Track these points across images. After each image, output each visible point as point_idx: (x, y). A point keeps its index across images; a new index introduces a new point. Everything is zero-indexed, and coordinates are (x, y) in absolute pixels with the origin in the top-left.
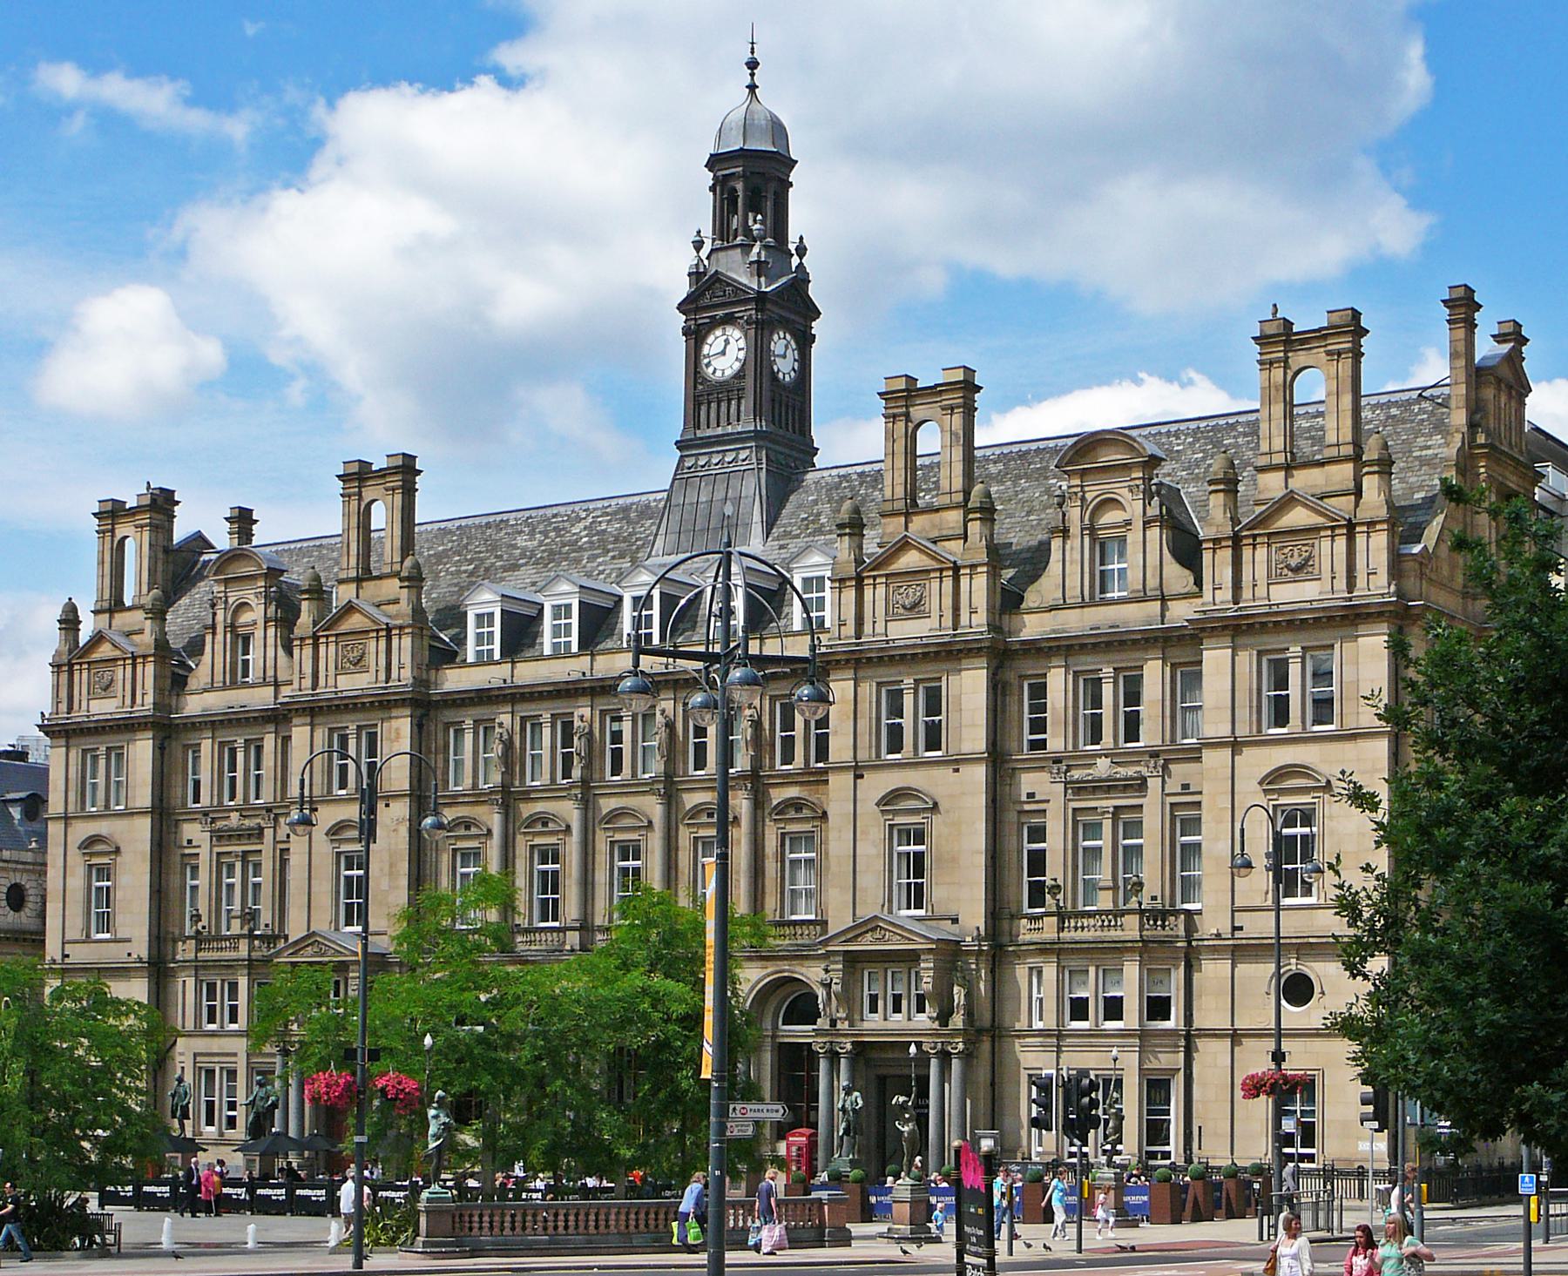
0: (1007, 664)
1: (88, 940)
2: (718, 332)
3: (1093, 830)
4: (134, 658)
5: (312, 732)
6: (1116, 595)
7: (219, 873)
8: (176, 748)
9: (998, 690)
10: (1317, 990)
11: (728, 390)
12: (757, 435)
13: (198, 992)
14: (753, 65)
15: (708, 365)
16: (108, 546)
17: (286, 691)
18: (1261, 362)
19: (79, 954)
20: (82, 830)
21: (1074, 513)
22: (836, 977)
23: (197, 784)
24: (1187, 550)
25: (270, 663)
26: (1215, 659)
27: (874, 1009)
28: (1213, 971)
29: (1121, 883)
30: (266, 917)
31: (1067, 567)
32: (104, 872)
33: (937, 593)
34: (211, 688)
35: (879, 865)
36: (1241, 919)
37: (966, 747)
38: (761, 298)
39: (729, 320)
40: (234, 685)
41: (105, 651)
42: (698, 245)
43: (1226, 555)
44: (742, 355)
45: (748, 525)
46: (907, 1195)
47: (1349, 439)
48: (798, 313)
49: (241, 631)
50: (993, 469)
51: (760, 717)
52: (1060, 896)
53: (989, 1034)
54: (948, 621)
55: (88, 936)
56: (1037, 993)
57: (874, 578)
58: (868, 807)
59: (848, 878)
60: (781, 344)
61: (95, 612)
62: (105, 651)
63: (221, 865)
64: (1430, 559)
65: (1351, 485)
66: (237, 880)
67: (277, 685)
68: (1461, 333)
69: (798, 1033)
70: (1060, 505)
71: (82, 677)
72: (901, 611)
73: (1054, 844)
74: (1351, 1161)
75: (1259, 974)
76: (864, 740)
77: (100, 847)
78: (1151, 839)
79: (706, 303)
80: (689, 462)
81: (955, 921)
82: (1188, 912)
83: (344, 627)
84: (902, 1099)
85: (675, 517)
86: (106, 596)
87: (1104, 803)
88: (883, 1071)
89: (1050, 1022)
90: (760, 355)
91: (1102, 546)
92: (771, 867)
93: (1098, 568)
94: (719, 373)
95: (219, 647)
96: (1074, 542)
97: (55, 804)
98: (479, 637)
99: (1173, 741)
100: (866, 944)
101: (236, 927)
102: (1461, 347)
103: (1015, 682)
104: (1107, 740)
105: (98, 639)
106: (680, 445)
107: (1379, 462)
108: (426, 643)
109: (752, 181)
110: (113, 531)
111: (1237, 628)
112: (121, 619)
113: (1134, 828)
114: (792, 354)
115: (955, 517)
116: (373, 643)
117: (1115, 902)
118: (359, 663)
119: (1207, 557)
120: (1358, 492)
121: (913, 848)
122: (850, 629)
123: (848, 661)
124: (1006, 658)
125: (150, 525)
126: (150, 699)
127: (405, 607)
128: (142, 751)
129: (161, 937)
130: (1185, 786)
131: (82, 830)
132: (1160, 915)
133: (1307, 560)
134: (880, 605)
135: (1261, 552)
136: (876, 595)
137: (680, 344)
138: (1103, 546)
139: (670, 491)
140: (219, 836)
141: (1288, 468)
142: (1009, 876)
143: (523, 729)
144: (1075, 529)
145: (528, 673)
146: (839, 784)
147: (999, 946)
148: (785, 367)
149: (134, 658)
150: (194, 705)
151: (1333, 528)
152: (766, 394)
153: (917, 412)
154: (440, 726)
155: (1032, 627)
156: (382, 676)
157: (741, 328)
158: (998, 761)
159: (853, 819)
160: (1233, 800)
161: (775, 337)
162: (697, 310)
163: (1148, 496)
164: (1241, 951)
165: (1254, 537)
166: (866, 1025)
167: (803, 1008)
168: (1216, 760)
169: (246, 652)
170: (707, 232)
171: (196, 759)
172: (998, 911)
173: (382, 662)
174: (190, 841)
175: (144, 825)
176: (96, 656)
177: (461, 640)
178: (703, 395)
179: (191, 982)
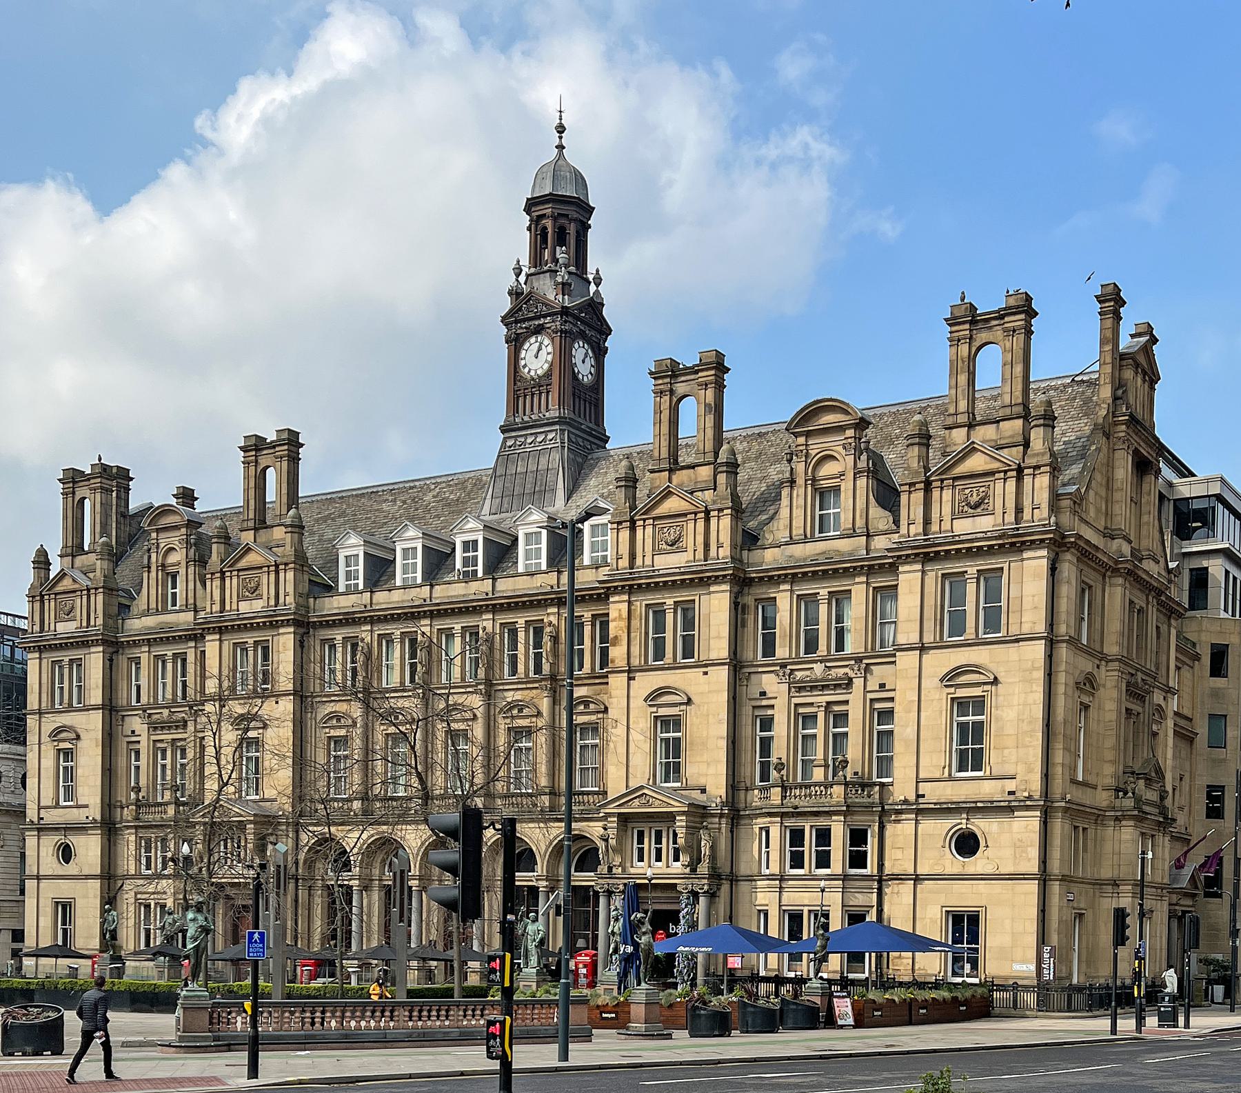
1: (57, 806)
2: (533, 340)
3: (810, 719)
4: (88, 590)
5: (1053, 569)
6: (832, 533)
7: (155, 756)
8: (122, 661)
9: (738, 609)
10: (982, 843)
11: (541, 384)
12: (561, 421)
13: (138, 848)
14: (561, 129)
15: (525, 366)
16: (70, 505)
17: (202, 614)
18: (950, 340)
19: (51, 817)
20: (51, 722)
21: (800, 468)
22: (612, 833)
23: (138, 687)
24: (887, 496)
25: (191, 594)
26: (909, 578)
27: (641, 859)
29: (830, 762)
30: (190, 786)
31: (793, 511)
32: (68, 754)
33: (693, 532)
34: (792, 541)
35: (647, 747)
36: (924, 788)
37: (713, 655)
38: (565, 311)
39: (539, 330)
40: (165, 611)
41: (66, 584)
43: (918, 496)
44: (550, 358)
45: (554, 491)
46: (643, 998)
47: (1020, 401)
49: (170, 570)
51: (557, 633)
52: (784, 772)
53: (725, 879)
54: (1010, 517)
55: (57, 803)
56: (764, 847)
57: (644, 520)
58: (638, 702)
59: (625, 761)
61: (61, 556)
62: (66, 584)
63: (158, 750)
64: (1082, 500)
65: (1020, 439)
66: (168, 761)
67: (196, 611)
68: (1109, 323)
69: (583, 879)
70: (790, 461)
71: (50, 606)
72: (665, 546)
73: (780, 730)
74: (1006, 978)
75: (939, 829)
77: (63, 735)
78: (854, 729)
79: (522, 319)
80: (509, 443)
81: (703, 791)
82: (882, 785)
84: (639, 915)
85: (499, 484)
86: (70, 544)
87: (819, 699)
89: (775, 869)
90: (564, 356)
91: (822, 494)
93: (818, 513)
94: (532, 373)
95: (153, 582)
96: (799, 491)
97: (32, 702)
98: (348, 574)
99: (873, 649)
100: (635, 808)
101: (168, 796)
102: (1109, 334)
104: (822, 649)
105: (62, 575)
106: (504, 430)
107: (1044, 417)
108: (306, 577)
109: (561, 219)
110: (74, 493)
111: (927, 554)
112: (79, 560)
114: (590, 361)
115: (705, 472)
117: (826, 777)
118: (255, 592)
119: (904, 498)
120: (1026, 444)
122: (624, 563)
124: (744, 583)
125: (102, 488)
126: (100, 621)
127: (289, 550)
128: (95, 661)
129: (109, 803)
130: (882, 686)
131: (51, 722)
132: (864, 785)
133: (983, 499)
134: (649, 542)
135: (947, 494)
136: (645, 535)
137: (504, 350)
138: (824, 494)
139: (495, 469)
140: (154, 727)
141: (971, 426)
142: (745, 757)
143: (380, 645)
144: (800, 481)
145: (384, 599)
146: (617, 682)
147: (735, 814)
148: (585, 370)
149: (88, 590)
150: (136, 625)
151: (1005, 472)
153: (681, 388)
154: (318, 642)
155: (770, 558)
156: (272, 602)
157: (549, 335)
158: (737, 667)
159: (627, 709)
160: (919, 697)
161: (576, 345)
163: (858, 453)
164: (921, 810)
165: (942, 481)
166: (632, 871)
167: (589, 859)
168: (907, 661)
169: (174, 587)
170: (525, 262)
171: (138, 669)
172: (734, 784)
173: (1011, 505)
174: (133, 732)
175: (97, 718)
177: (335, 579)
178: (520, 388)
179: (132, 838)
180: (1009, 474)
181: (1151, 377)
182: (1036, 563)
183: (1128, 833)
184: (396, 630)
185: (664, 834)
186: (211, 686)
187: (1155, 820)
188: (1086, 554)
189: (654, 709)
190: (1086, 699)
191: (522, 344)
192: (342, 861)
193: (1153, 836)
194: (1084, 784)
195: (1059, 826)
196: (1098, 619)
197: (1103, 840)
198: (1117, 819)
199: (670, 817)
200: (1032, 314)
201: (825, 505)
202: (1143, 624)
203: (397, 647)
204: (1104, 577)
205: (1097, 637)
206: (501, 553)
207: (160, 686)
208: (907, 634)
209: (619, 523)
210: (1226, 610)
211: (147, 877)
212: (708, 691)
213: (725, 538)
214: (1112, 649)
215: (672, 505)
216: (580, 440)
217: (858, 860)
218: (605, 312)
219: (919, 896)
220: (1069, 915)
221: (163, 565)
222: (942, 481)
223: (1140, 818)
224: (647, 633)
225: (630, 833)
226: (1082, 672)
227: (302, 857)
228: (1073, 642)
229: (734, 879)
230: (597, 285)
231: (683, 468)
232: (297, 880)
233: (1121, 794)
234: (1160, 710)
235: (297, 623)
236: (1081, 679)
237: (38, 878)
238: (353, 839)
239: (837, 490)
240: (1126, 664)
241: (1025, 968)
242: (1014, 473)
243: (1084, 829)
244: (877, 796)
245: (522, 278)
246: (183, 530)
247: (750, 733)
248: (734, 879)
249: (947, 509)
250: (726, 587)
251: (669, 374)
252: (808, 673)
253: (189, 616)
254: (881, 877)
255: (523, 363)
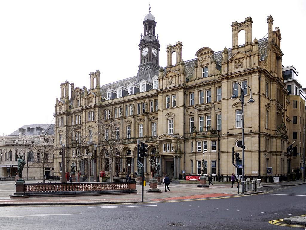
0: (187, 91)
3: (202, 118)
5: (259, 78)
11: (146, 57)
14: (150, 8)
21: (199, 63)
22: (158, 145)
26: (224, 84)
28: (224, 141)
36: (229, 131)
38: (150, 42)
39: (146, 47)
42: (142, 36)
43: (226, 65)
48: (157, 46)
50: (186, 64)
54: (248, 67)
58: (230, 107)
60: (154, 51)
70: (196, 62)
76: (163, 106)
79: (143, 44)
82: (219, 131)
83: (89, 97)
87: (204, 113)
88: (167, 160)
90: (150, 51)
92: (150, 128)
103: (188, 94)
105: (60, 102)
113: (209, 117)
116: (93, 98)
121: (171, 123)
123: (160, 92)
130: (218, 109)
135: (233, 64)
137: (139, 51)
142: (187, 127)
143: (114, 110)
144: (199, 66)
147: (185, 139)
151: (247, 57)
152: (152, 57)
153: (172, 50)
159: (162, 117)
161: (153, 49)
162: (141, 46)
164: (229, 136)
165: (231, 61)
172: (185, 133)
176: (60, 105)
178: (142, 58)
180: (248, 57)
181: (280, 38)
182: (255, 76)
183: (279, 141)
184: (117, 106)
185: (166, 145)
186: (84, 121)
187: (284, 138)
188: (267, 76)
189: (167, 118)
190: (268, 109)
191: (143, 49)
192: (129, 152)
193: (284, 141)
194: (267, 129)
195: (263, 139)
196: (270, 91)
197: (272, 142)
198: (276, 137)
199: (170, 141)
200: (252, 22)
201: (205, 71)
202: (280, 93)
203: (117, 110)
204: (271, 81)
205: (270, 95)
206: (137, 90)
207: (80, 121)
208: (224, 96)
209: (160, 79)
210: (295, 94)
211: (74, 157)
212: (179, 113)
213: (182, 80)
214: (273, 98)
215: (170, 74)
216: (154, 68)
217: (214, 148)
218: (159, 43)
219: (228, 156)
220: (265, 159)
221: (77, 99)
222: (231, 61)
223: (282, 137)
224: (166, 102)
225: (162, 144)
226: (267, 103)
227: (100, 152)
228: (264, 95)
229: (185, 153)
230: (158, 37)
231: (173, 67)
232: (99, 157)
233: (277, 131)
234: (283, 114)
235: (66, 114)
236: (267, 104)
237: (56, 158)
238: (120, 148)
239: (207, 67)
240: (277, 102)
241: (255, 172)
242: (249, 57)
243: (268, 140)
244: (218, 134)
245: (143, 37)
246: (210, 54)
247: (189, 122)
248: (185, 153)
249: (233, 67)
250: (183, 90)
251: (170, 49)
252: (201, 107)
253: (81, 108)
254: (219, 152)
255: (142, 53)
